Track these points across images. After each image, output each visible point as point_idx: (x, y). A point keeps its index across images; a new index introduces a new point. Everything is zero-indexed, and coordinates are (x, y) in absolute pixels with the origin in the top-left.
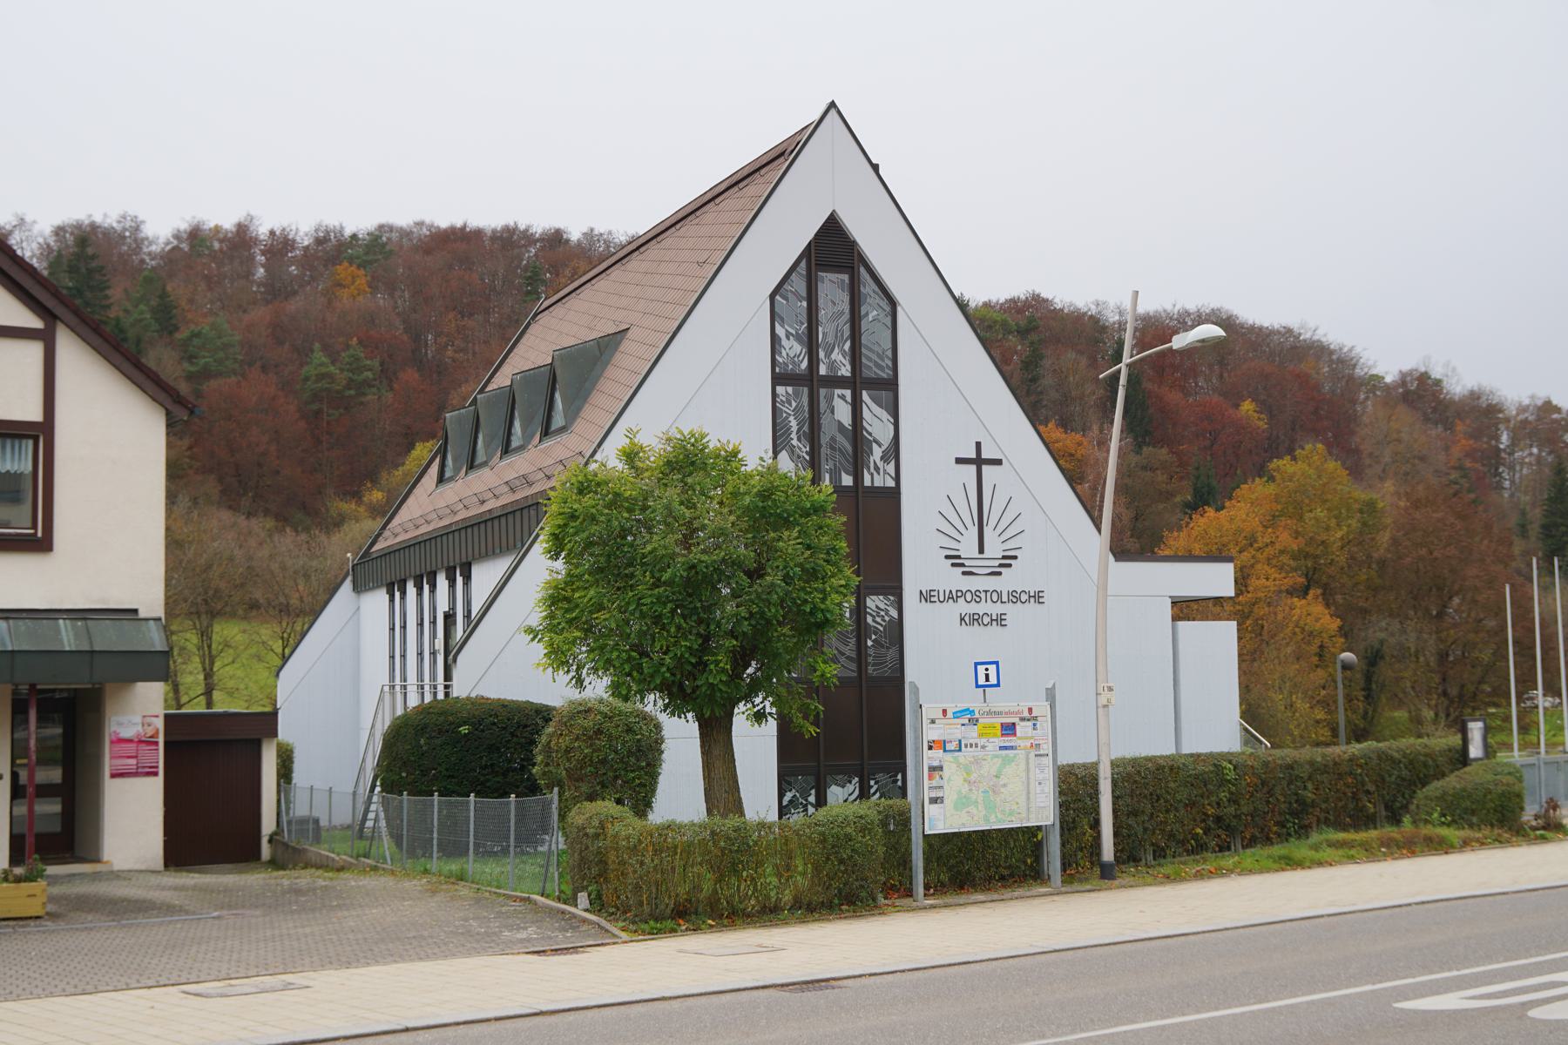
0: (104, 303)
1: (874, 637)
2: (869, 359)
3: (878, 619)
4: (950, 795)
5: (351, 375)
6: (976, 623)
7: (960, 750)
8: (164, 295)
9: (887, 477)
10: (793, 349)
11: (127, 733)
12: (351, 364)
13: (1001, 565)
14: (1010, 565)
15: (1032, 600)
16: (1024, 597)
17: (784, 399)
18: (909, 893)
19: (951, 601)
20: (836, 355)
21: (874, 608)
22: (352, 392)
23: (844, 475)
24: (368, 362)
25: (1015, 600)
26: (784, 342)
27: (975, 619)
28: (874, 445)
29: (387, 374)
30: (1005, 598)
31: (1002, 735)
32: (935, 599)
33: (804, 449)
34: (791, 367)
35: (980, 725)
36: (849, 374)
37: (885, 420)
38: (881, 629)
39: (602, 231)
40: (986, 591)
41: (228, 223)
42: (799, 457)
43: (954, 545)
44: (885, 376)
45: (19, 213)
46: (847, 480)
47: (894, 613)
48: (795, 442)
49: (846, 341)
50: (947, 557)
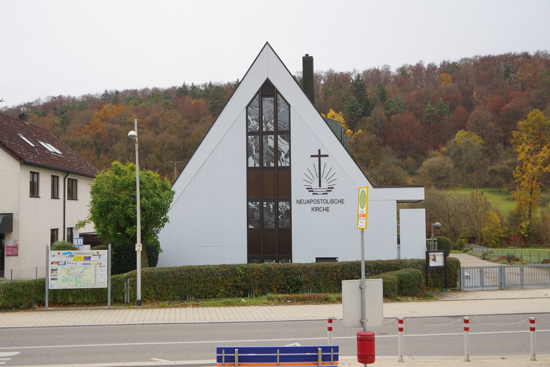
0: (365, 94)
1: (281, 215)
2: (281, 125)
3: (283, 209)
4: (60, 278)
5: (439, 110)
6: (317, 210)
7: (65, 264)
8: (383, 90)
9: (286, 163)
10: (254, 124)
11: (10, 245)
12: (440, 106)
13: (327, 191)
14: (331, 191)
15: (339, 202)
16: (336, 201)
17: (251, 140)
18: (44, 305)
19: (308, 203)
20: (269, 124)
21: (281, 206)
22: (440, 115)
23: (271, 163)
24: (446, 105)
25: (332, 202)
26: (251, 122)
27: (317, 209)
28: (282, 153)
29: (453, 108)
30: (329, 202)
31: (84, 260)
32: (303, 203)
33: (257, 156)
34: (253, 129)
35: (74, 257)
36: (273, 130)
37: (286, 144)
38: (284, 213)
39: (542, 51)
40: (322, 200)
41: (414, 64)
42: (256, 158)
43: (310, 184)
44: (286, 130)
45: (354, 68)
46: (272, 165)
47: (289, 207)
48: (254, 153)
49: (272, 119)
50: (307, 189)
